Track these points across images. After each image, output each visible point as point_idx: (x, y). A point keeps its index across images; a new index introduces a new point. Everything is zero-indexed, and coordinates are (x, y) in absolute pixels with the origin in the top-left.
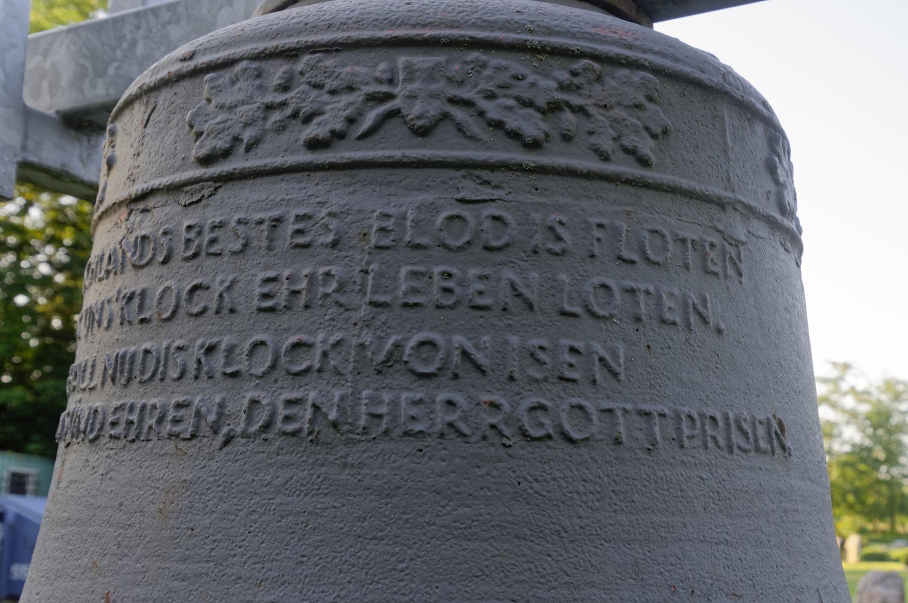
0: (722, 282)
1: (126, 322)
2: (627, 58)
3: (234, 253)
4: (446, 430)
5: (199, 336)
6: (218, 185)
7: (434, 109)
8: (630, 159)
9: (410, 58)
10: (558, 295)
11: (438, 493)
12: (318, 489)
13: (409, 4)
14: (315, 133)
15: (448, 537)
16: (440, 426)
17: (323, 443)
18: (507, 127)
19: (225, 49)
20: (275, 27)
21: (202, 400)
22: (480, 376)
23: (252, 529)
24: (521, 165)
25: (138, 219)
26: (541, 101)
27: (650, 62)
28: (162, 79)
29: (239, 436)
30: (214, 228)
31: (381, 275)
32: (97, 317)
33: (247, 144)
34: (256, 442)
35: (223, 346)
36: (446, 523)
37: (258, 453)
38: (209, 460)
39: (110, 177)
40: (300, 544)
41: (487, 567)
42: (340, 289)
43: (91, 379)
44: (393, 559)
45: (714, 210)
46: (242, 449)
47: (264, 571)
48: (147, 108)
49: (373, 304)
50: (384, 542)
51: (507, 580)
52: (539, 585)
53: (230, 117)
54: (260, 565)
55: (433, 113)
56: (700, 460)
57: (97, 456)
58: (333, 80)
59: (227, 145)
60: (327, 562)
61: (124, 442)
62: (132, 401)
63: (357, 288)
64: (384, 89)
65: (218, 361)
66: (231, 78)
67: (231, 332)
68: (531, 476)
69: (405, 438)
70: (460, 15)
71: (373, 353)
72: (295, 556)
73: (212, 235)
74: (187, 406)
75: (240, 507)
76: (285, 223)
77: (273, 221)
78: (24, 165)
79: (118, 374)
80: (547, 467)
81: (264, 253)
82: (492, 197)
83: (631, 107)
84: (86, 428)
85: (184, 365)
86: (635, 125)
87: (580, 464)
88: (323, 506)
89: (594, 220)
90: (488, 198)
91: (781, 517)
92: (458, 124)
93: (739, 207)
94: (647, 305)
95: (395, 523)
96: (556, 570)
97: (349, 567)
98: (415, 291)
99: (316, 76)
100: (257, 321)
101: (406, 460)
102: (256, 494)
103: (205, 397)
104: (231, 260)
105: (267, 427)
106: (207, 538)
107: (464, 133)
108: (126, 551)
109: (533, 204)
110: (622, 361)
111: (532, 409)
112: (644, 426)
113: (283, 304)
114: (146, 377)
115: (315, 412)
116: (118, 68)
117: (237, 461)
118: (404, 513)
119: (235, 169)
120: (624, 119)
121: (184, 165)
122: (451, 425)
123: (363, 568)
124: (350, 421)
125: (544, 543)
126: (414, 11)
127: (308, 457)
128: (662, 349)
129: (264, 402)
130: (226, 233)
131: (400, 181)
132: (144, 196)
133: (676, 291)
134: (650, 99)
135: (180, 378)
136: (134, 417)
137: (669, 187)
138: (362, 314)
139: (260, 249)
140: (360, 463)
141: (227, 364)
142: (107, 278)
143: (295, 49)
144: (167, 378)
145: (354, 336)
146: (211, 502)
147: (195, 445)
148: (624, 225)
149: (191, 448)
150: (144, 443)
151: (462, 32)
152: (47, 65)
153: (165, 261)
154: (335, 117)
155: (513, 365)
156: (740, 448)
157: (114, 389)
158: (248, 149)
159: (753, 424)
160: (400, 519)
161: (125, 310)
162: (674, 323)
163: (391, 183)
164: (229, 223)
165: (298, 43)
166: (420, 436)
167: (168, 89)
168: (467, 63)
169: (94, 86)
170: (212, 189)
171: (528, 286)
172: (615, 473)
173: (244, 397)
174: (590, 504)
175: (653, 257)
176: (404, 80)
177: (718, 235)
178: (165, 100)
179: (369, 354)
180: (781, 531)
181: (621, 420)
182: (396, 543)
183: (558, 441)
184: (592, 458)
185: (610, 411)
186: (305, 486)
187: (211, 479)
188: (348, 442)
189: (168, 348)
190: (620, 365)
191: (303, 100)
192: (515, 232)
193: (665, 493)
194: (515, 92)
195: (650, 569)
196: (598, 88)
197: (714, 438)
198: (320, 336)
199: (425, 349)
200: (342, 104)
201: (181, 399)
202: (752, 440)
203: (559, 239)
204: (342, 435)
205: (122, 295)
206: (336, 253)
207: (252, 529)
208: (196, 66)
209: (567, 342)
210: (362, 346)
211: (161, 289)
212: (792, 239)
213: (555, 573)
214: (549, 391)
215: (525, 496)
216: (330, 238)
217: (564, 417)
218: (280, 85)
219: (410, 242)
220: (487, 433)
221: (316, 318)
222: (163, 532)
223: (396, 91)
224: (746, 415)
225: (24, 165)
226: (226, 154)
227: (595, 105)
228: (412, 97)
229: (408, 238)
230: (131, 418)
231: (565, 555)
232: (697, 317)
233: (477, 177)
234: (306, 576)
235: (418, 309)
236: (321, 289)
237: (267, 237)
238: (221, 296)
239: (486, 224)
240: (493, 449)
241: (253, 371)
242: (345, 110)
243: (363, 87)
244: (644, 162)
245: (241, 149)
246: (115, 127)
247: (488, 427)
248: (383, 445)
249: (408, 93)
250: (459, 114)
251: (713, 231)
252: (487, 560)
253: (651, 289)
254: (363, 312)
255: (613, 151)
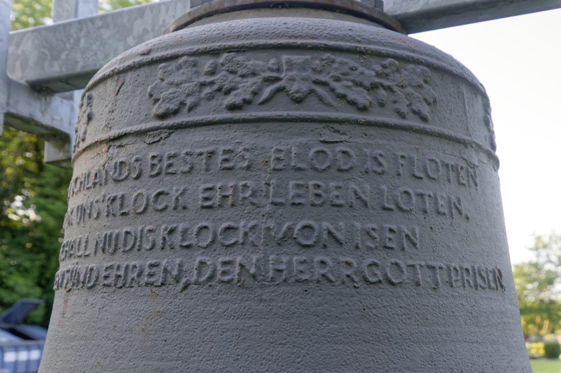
0: (467, 189)
1: (111, 215)
2: (413, 58)
3: (184, 173)
4: (321, 279)
5: (163, 223)
6: (171, 131)
7: (305, 87)
8: (416, 117)
9: (289, 57)
10: (381, 198)
11: (318, 316)
12: (245, 315)
13: (285, 24)
14: (233, 100)
15: (325, 342)
16: (317, 276)
17: (247, 287)
18: (348, 98)
19: (171, 49)
20: (203, 36)
21: (167, 262)
22: (339, 246)
23: (204, 340)
24: (357, 121)
25: (116, 151)
26: (367, 83)
27: (425, 61)
28: (129, 66)
29: (193, 284)
30: (170, 157)
31: (278, 186)
32: (88, 211)
33: (189, 107)
34: (204, 287)
35: (180, 229)
36: (323, 334)
37: (206, 294)
38: (174, 298)
39: (90, 125)
40: (236, 348)
41: (348, 359)
42: (253, 194)
43: (85, 250)
44: (293, 356)
45: (461, 147)
46: (195, 291)
47: (214, 365)
48: (118, 83)
49: (273, 203)
50: (287, 346)
51: (360, 367)
52: (379, 370)
53: (178, 90)
54: (211, 362)
55: (305, 89)
56: (461, 294)
57: (94, 297)
58: (243, 69)
59: (176, 107)
60: (253, 359)
61: (114, 288)
62: (118, 263)
63: (264, 194)
64: (275, 74)
65: (177, 238)
66: (176, 67)
67: (184, 221)
68: (371, 305)
69: (296, 284)
70: (317, 31)
71: (275, 233)
72: (233, 356)
73: (169, 162)
74: (157, 266)
75: (196, 327)
76: (217, 155)
77: (209, 153)
78: (8, 115)
79: (107, 247)
80: (379, 300)
81: (204, 173)
82: (341, 140)
83: (416, 86)
84: (85, 280)
85: (154, 241)
86: (419, 98)
87: (398, 298)
88: (249, 325)
89: (399, 153)
90: (338, 140)
91: (503, 327)
92: (320, 96)
93: (474, 145)
94: (430, 203)
95: (293, 334)
96: (388, 360)
97: (267, 361)
98: (298, 196)
99: (232, 66)
100: (201, 214)
101: (298, 297)
102: (206, 318)
103: (170, 260)
104: (182, 177)
105: (211, 278)
106: (176, 346)
107: (323, 101)
108: (121, 355)
109: (364, 144)
110: (418, 237)
111: (370, 265)
112: (431, 275)
113: (218, 204)
114: (128, 248)
115: (241, 269)
116: (67, 55)
117: (192, 299)
118: (298, 328)
119: (183, 122)
120: (413, 94)
121: (147, 119)
122: (323, 275)
123: (275, 362)
124: (263, 274)
125: (380, 345)
126: (289, 28)
127: (238, 296)
128: (439, 229)
129: (209, 263)
130: (178, 161)
131: (286, 130)
132: (119, 137)
133: (444, 195)
134: (426, 82)
135: (152, 248)
136: (121, 273)
137: (438, 133)
138: (268, 209)
139: (201, 170)
140: (270, 299)
141: (183, 240)
142: (94, 188)
143: (217, 50)
144: (142, 249)
145: (263, 223)
146: (177, 324)
147: (164, 290)
148: (416, 156)
149: (162, 292)
150: (128, 289)
151: (320, 42)
152: (19, 52)
153: (137, 178)
154: (245, 91)
155: (358, 240)
156: (481, 286)
157: (104, 256)
158: (190, 110)
159: (487, 272)
160: (296, 332)
161: (110, 208)
162: (444, 214)
163: (280, 131)
164: (180, 154)
165: (219, 46)
166: (305, 282)
167: (133, 72)
168: (323, 60)
169: (51, 65)
170: (167, 134)
171: (364, 193)
172: (417, 302)
173: (195, 260)
174: (404, 321)
175: (431, 175)
176: (287, 69)
177: (464, 162)
178: (131, 78)
179: (273, 233)
180: (503, 335)
181: (419, 271)
182: (294, 346)
183: (385, 285)
184: (404, 294)
185: (413, 266)
186: (237, 313)
187: (176, 310)
188: (262, 287)
189: (142, 231)
190: (417, 239)
191: (225, 81)
192: (355, 160)
193: (444, 314)
194: (351, 77)
195: (439, 359)
196: (398, 75)
197: (468, 281)
198: (242, 223)
199: (306, 230)
200: (249, 84)
201: (153, 262)
202: (487, 282)
203: (380, 165)
204: (258, 282)
205: (107, 198)
206: (249, 173)
207: (204, 340)
208: (152, 59)
209: (388, 226)
210: (268, 229)
211: (135, 194)
212: (496, 162)
213: (387, 362)
214: (379, 254)
215: (368, 317)
216: (246, 164)
217: (388, 270)
218: (209, 71)
219: (294, 166)
220: (345, 280)
221: (239, 212)
222: (146, 343)
223: (282, 76)
224: (483, 267)
225: (8, 115)
226: (176, 112)
227: (397, 85)
228: (292, 80)
229: (293, 164)
230: (119, 273)
231: (392, 352)
232: (456, 210)
233: (332, 128)
234: (240, 368)
235: (301, 206)
236: (241, 194)
237: (206, 163)
238: (177, 199)
239: (338, 156)
240: (348, 289)
241: (200, 244)
242: (251, 87)
243: (261, 73)
244: (424, 119)
245: (186, 109)
246: (91, 94)
247: (345, 277)
248: (283, 288)
249: (289, 78)
250: (320, 90)
251: (462, 160)
252: (348, 355)
253: (432, 194)
254: (268, 208)
255: (407, 113)
